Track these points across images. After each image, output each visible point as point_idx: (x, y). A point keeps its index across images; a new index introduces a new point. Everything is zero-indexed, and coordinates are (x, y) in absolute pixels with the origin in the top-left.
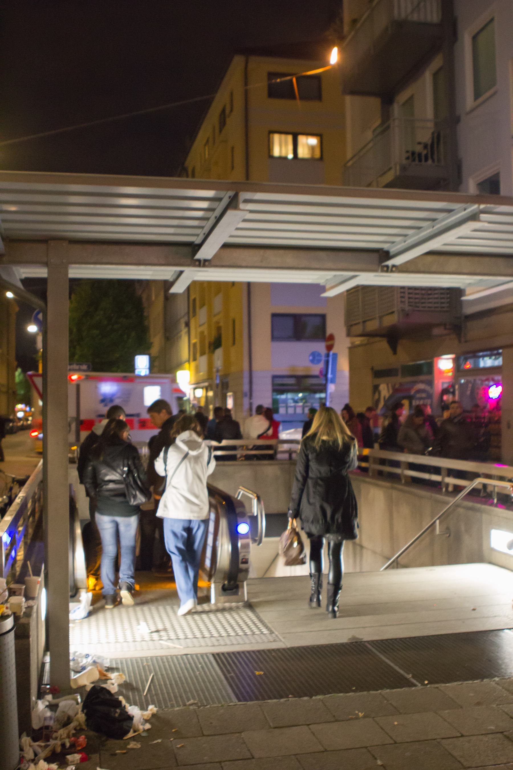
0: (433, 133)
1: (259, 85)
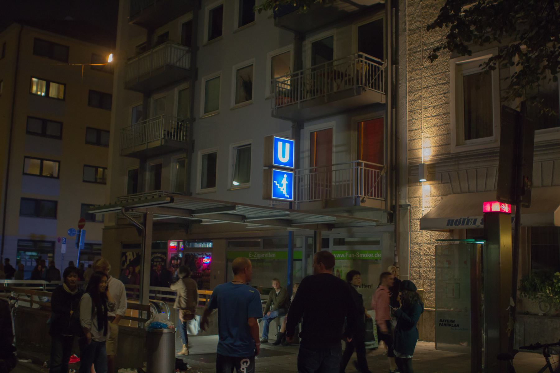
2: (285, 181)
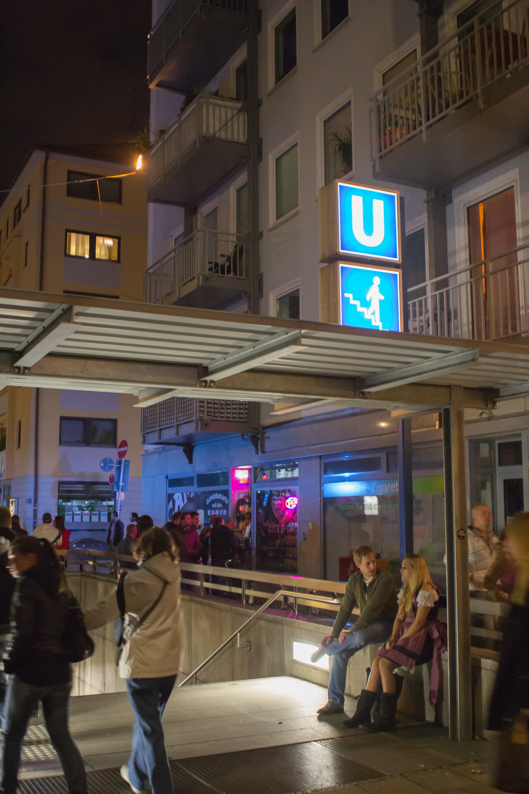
0: (235, 247)
1: (59, 184)
2: (375, 294)
